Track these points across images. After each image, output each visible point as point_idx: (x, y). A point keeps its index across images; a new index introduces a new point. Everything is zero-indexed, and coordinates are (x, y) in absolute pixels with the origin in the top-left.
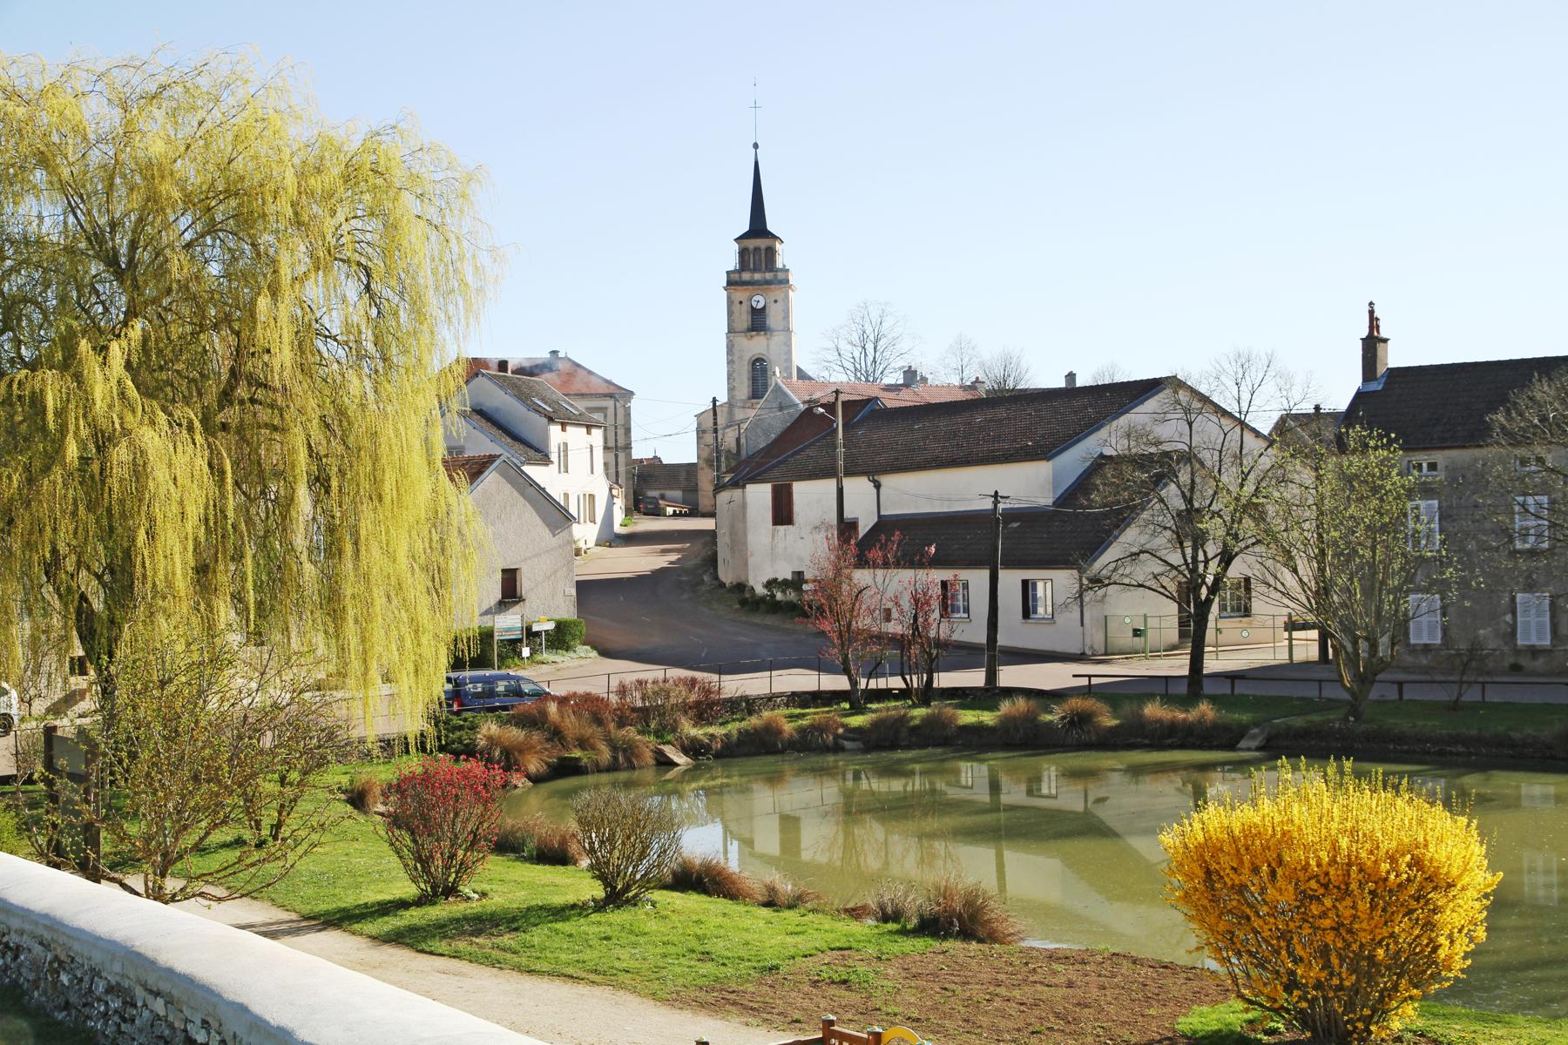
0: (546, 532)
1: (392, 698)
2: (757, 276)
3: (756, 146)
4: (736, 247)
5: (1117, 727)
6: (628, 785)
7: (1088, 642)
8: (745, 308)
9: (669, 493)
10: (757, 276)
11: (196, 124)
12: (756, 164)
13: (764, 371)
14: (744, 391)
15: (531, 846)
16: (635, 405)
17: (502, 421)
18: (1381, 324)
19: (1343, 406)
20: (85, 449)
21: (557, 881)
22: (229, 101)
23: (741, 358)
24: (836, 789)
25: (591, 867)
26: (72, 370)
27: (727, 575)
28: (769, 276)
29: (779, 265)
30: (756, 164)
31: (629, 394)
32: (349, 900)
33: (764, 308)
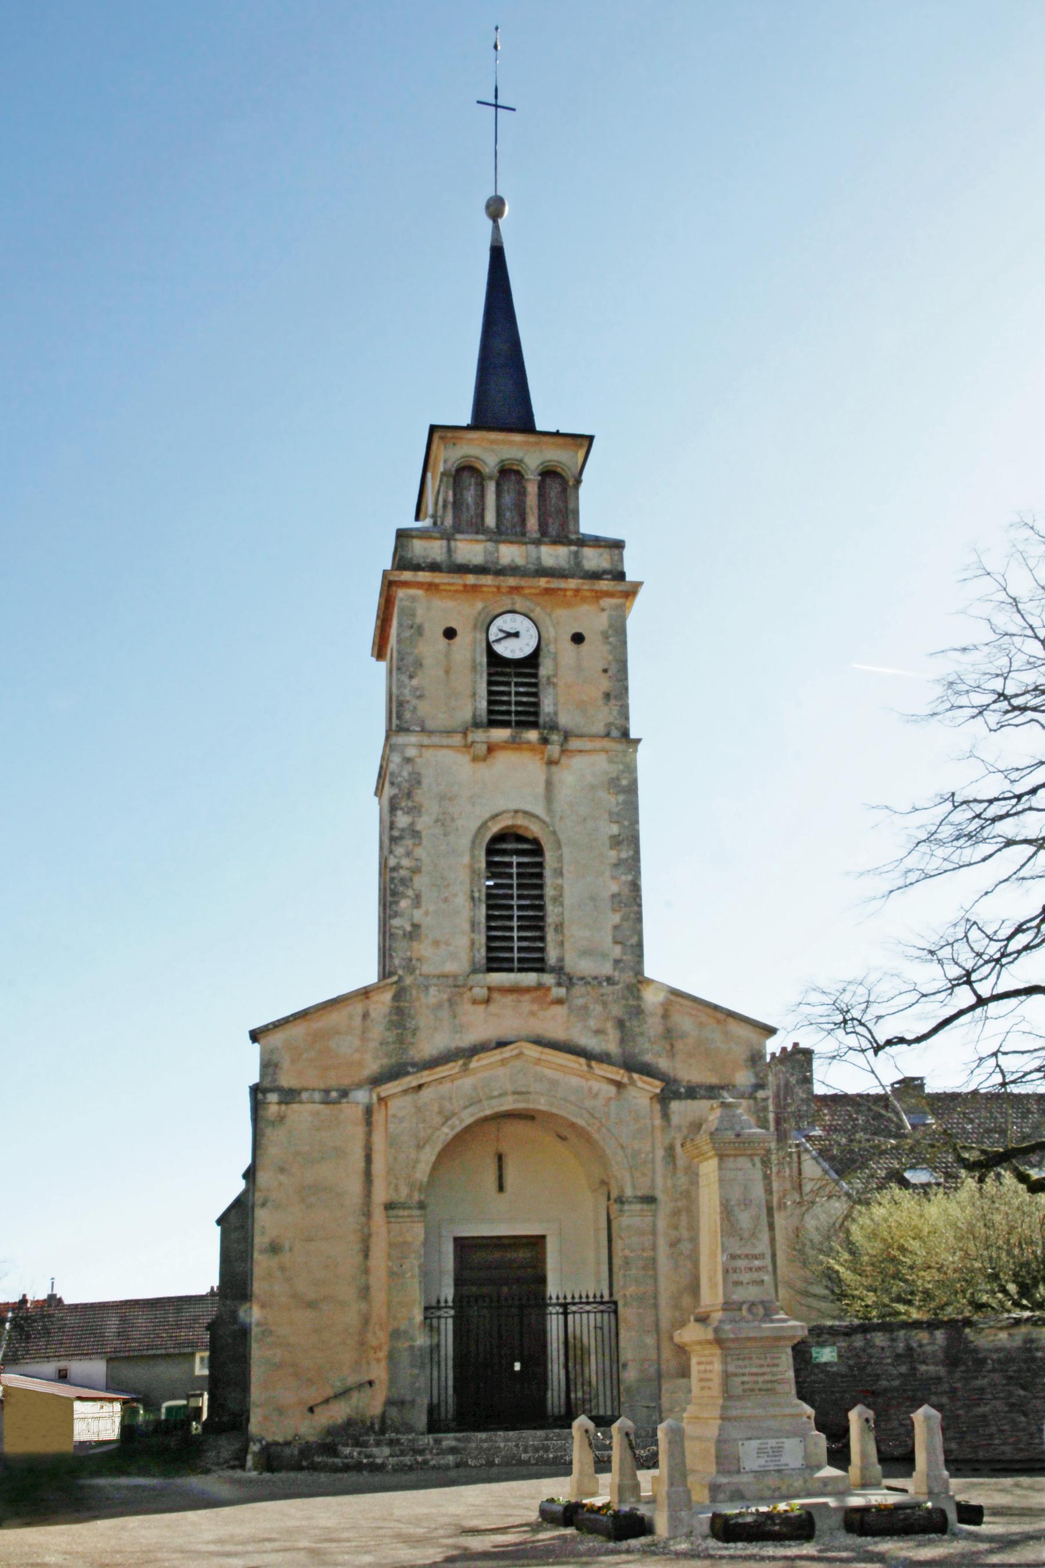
0: (568, 1478)
1: (918, 1208)
2: (509, 553)
3: (495, 208)
4: (218, 1229)
5: (210, 1394)
6: (902, 1249)
7: (478, 713)
8: (467, 650)
9: (78, 1367)
10: (509, 553)
11: (425, 1092)
12: (497, 255)
13: (533, 877)
14: (454, 930)
15: (493, 1045)
16: (626, 553)
17: (743, 1024)
18: (890, 1037)
19: (215, 1281)
20: (396, 1189)
21: (437, 581)
22: (1034, 1345)
23: (443, 822)
24: (439, 559)
25: (361, 1463)
26: (952, 1516)
27: (458, 536)
28: (552, 555)
29: (588, 525)
30: (497, 255)
31: (602, 633)
32: (497, 1056)
33: (533, 660)
